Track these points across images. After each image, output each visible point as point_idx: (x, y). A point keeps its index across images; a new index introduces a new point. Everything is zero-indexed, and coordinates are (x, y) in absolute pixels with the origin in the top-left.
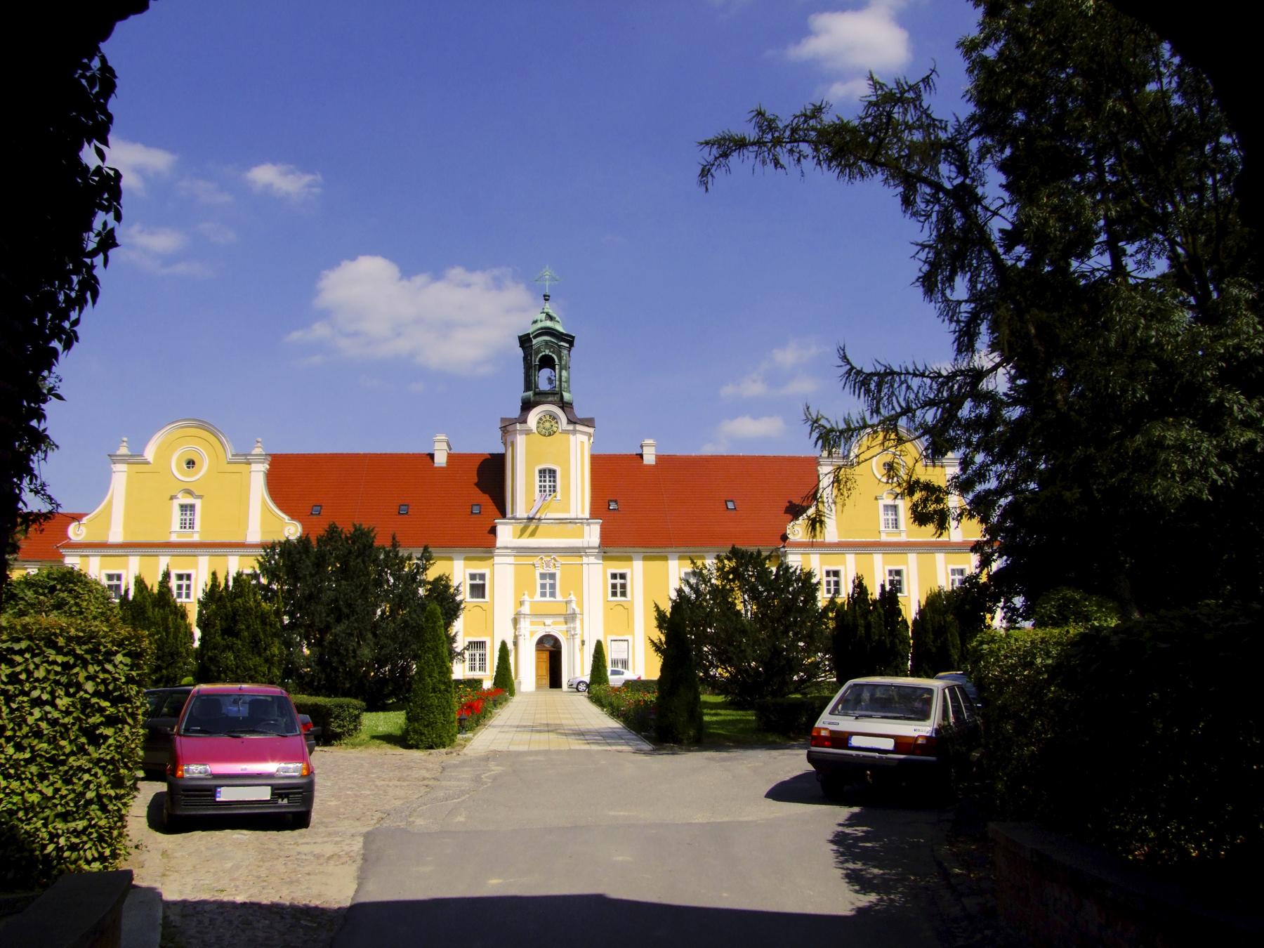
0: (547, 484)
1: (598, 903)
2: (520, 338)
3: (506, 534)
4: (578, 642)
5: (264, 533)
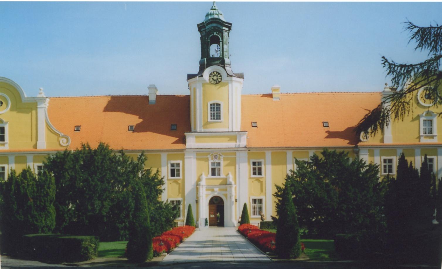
0: (218, 107)
1: (173, 96)
2: (198, 25)
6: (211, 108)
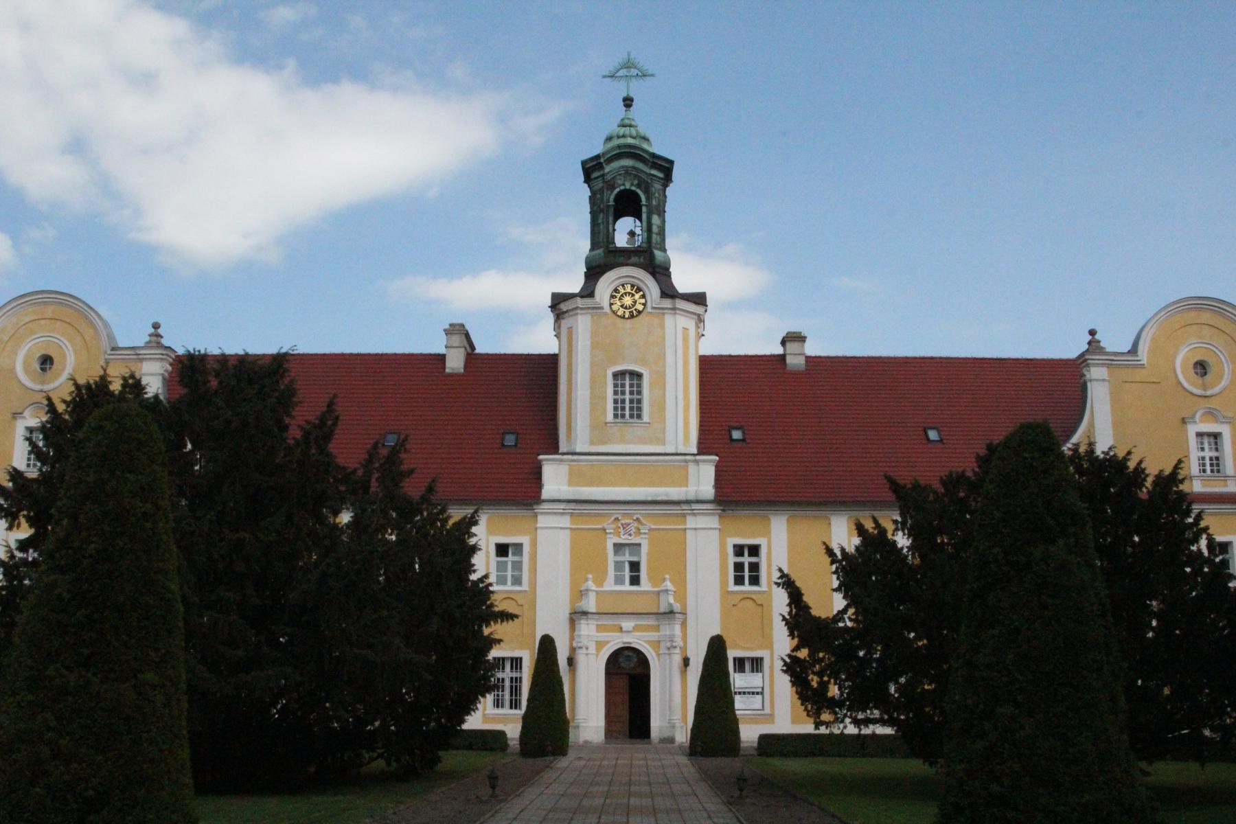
2: (584, 163)
3: (556, 479)
4: (677, 659)
6: (616, 386)
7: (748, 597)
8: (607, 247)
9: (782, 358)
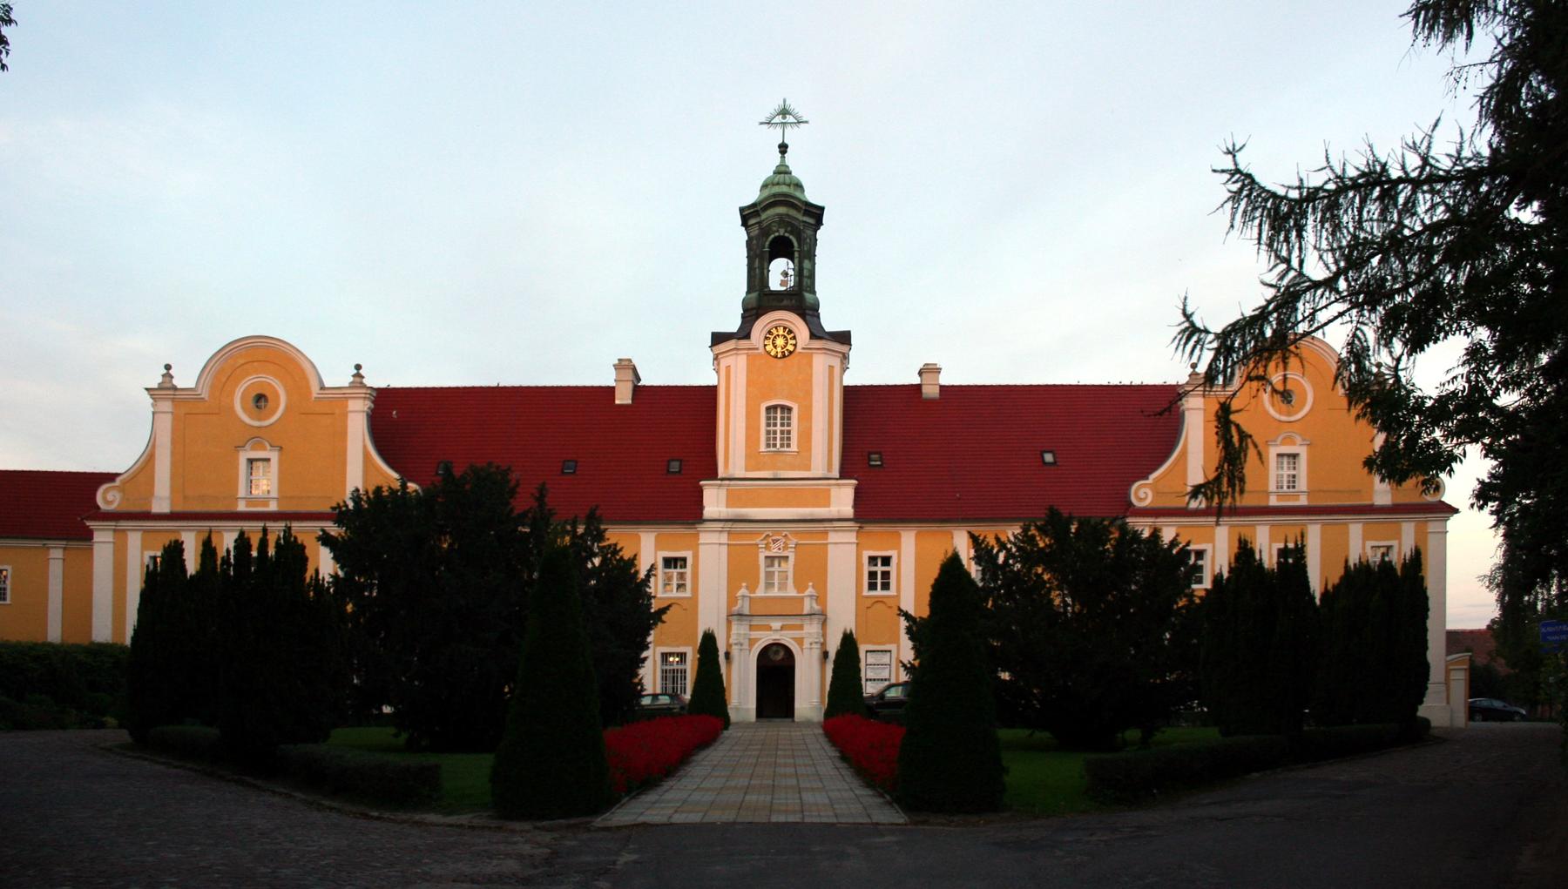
0: (778, 428)
2: (742, 210)
3: (714, 501)
5: (172, 502)
6: (768, 418)
7: (879, 601)
8: (761, 290)
9: (918, 387)
